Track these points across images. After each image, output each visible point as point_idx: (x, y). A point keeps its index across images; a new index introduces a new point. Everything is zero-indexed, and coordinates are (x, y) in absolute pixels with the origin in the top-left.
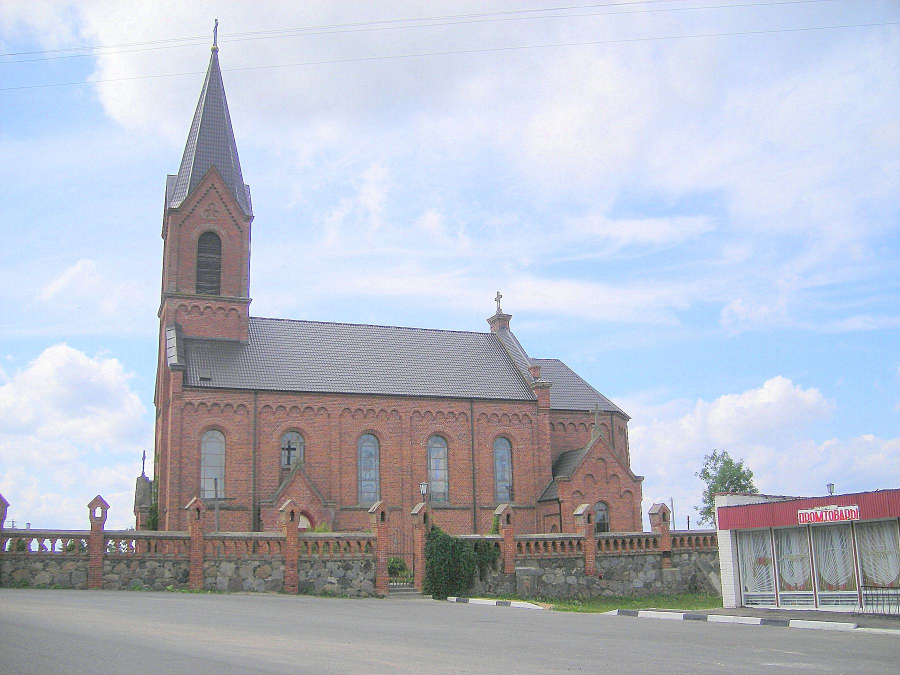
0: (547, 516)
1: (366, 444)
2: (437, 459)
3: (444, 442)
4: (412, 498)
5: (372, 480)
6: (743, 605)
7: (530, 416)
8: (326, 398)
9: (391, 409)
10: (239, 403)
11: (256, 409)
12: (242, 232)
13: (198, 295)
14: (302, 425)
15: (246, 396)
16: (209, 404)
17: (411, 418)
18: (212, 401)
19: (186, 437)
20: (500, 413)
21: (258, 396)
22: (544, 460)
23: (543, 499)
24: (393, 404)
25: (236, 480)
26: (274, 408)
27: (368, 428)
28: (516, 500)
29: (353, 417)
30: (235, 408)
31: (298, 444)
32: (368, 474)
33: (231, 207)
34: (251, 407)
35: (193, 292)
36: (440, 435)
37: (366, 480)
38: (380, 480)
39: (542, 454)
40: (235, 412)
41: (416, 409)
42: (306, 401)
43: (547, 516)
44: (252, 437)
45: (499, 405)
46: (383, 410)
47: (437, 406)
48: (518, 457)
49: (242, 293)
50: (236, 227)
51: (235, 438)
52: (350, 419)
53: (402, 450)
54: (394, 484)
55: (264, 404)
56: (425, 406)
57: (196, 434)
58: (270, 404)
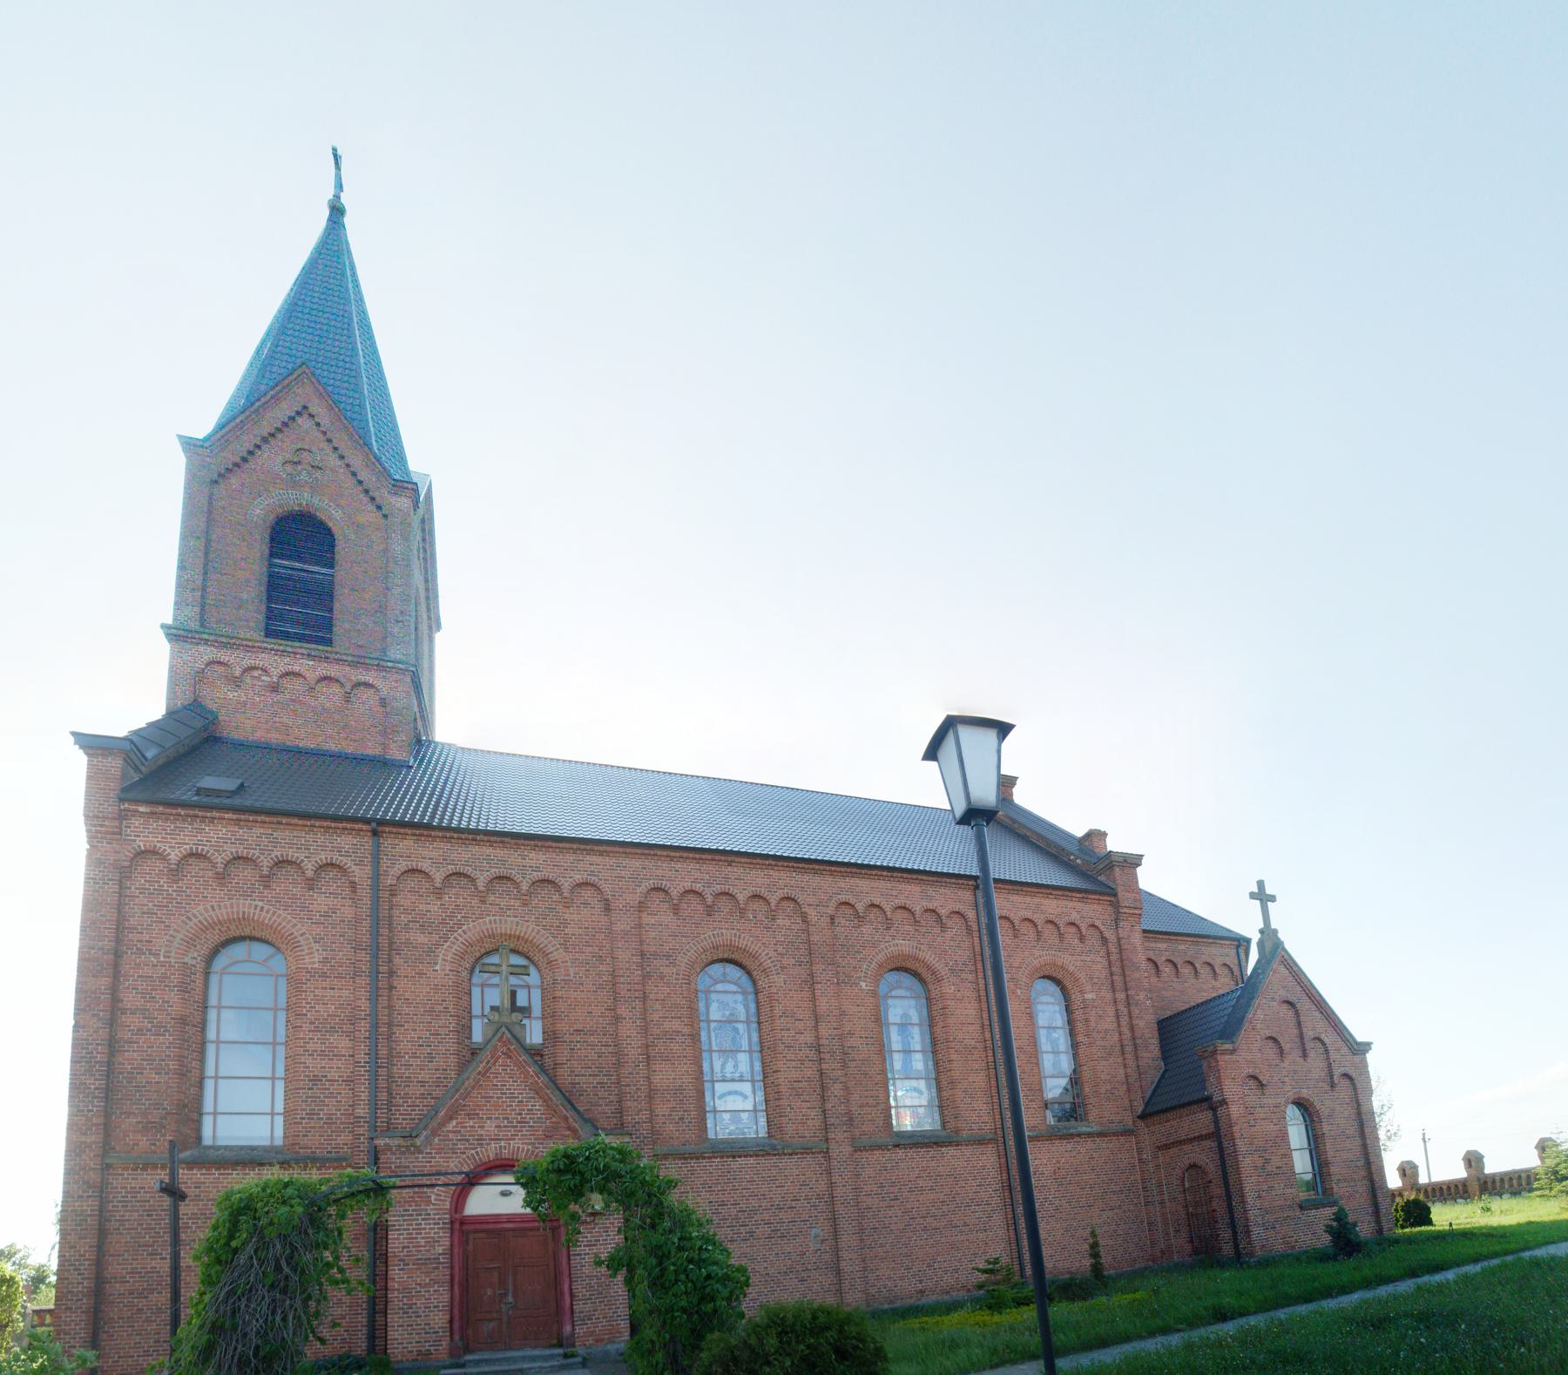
0: (1166, 1147)
1: (719, 987)
2: (903, 1026)
3: (917, 986)
4: (851, 1119)
5: (741, 1080)
6: (471, 1237)
7: (1102, 928)
8: (595, 859)
9: (780, 894)
10: (323, 857)
11: (377, 876)
12: (385, 516)
13: (268, 640)
14: (528, 929)
15: (346, 841)
16: (219, 860)
17: (832, 918)
18: (231, 850)
19: (140, 952)
20: (1039, 919)
21: (387, 843)
22: (1141, 1024)
23: (1151, 1109)
24: (786, 881)
25: (316, 1080)
26: (438, 877)
27: (719, 940)
28: (1091, 1118)
29: (676, 909)
30: (310, 874)
31: (504, 967)
32: (729, 1067)
33: (357, 461)
34: (361, 874)
35: (258, 635)
36: (904, 967)
37: (724, 1080)
38: (765, 1077)
39: (1137, 1012)
40: (311, 884)
41: (843, 898)
42: (536, 862)
43: (1166, 1147)
44: (364, 957)
45: (1037, 900)
46: (756, 896)
47: (894, 893)
48: (1087, 1020)
49: (390, 651)
50: (371, 507)
51: (313, 960)
52: (668, 918)
53: (814, 999)
54: (800, 1085)
55: (403, 865)
56: (867, 891)
57: (175, 944)
58: (425, 865)
